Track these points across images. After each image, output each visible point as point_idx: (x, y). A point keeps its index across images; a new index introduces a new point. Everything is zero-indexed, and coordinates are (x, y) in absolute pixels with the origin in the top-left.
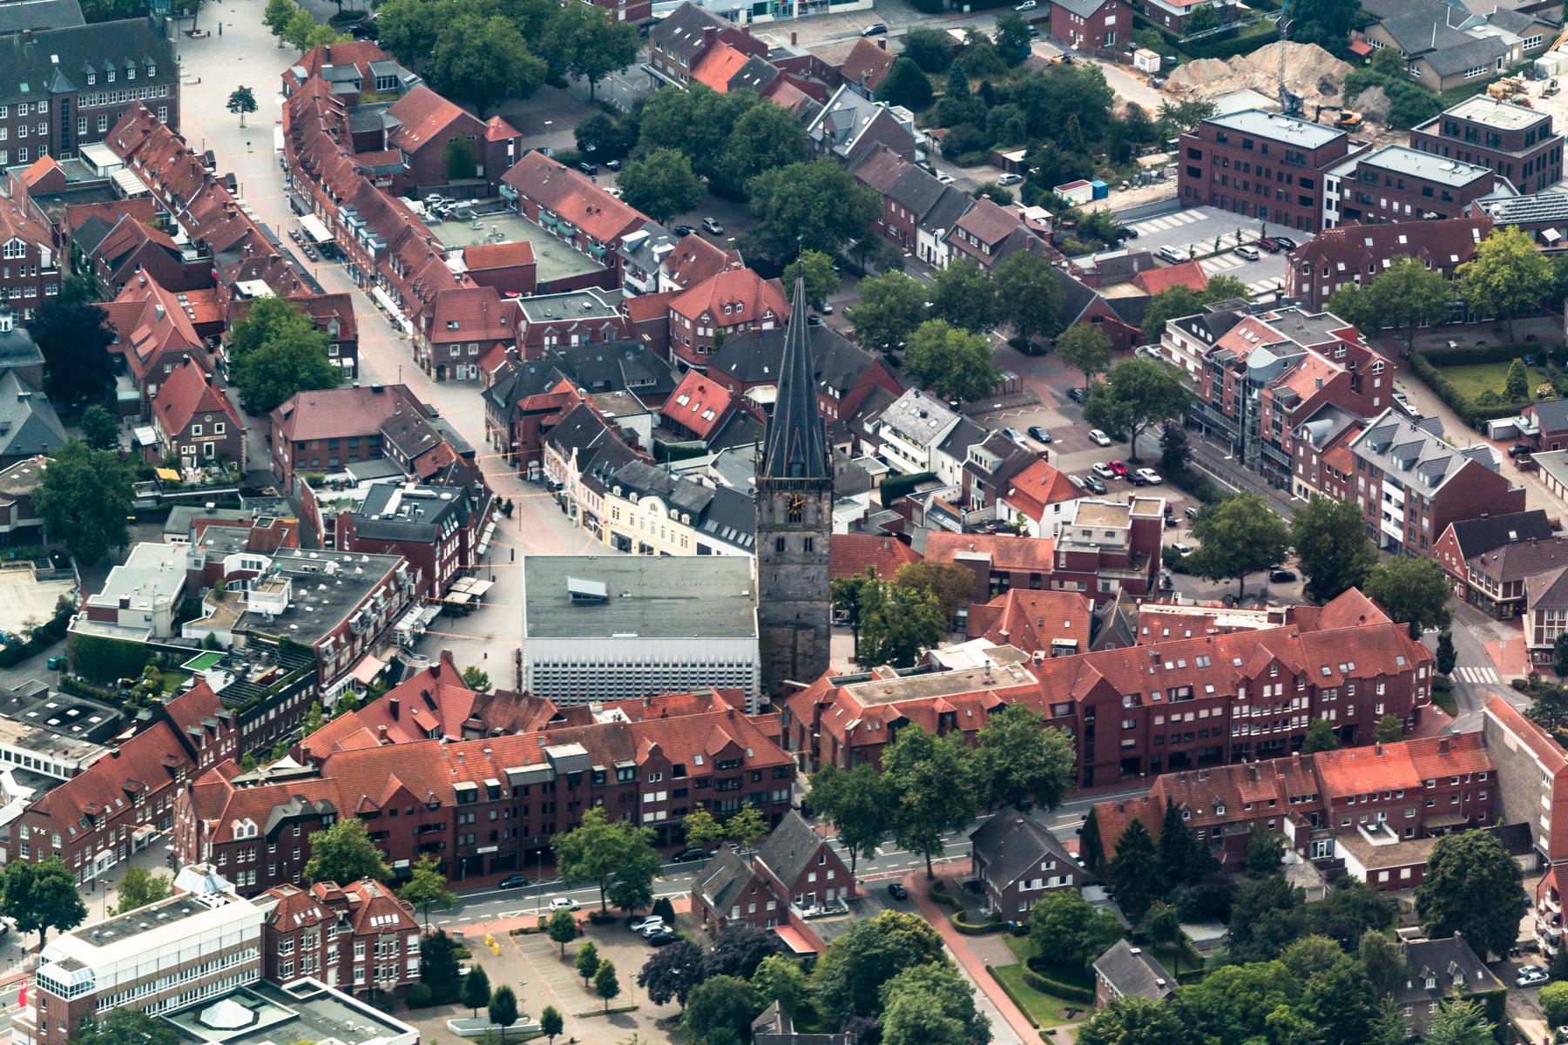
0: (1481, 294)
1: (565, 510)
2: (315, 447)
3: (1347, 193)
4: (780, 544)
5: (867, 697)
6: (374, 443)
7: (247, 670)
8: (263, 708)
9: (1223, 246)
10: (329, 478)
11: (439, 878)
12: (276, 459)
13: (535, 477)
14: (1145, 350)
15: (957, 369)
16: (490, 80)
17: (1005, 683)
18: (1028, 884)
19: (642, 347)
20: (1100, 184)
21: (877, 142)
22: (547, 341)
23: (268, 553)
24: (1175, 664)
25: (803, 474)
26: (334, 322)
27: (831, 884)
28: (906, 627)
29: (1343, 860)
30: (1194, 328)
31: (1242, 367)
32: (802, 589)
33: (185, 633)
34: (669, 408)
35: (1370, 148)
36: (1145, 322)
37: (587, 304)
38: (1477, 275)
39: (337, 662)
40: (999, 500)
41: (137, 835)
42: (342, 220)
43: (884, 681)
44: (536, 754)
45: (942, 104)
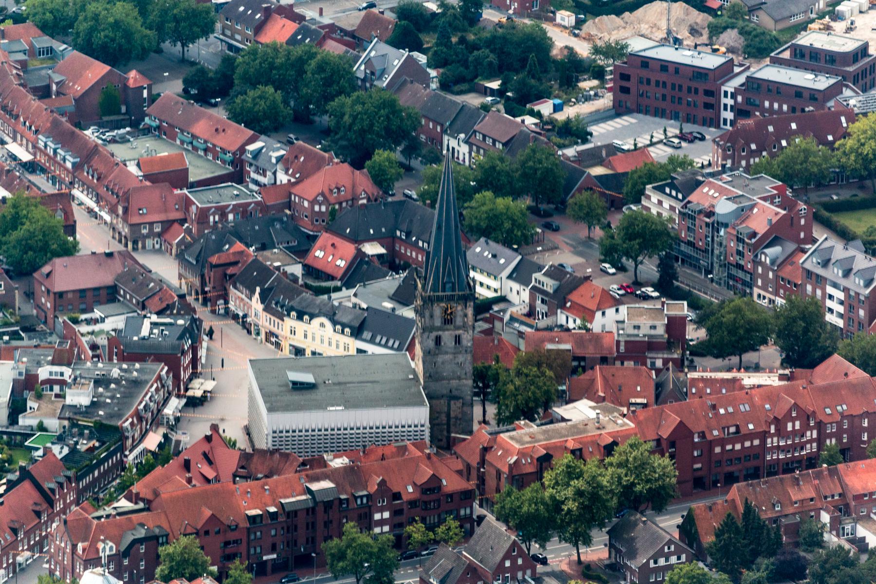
0: (855, 161)
1: (249, 332)
2: (70, 296)
3: (740, 99)
4: (438, 340)
5: (518, 441)
6: (110, 291)
7: (77, 443)
8: (91, 469)
9: (654, 140)
10: (83, 317)
11: (249, 575)
12: (39, 307)
13: (222, 311)
14: (630, 209)
15: (507, 225)
16: (120, 46)
17: (611, 428)
18: (656, 562)
19: (285, 219)
20: (558, 101)
21: (404, 77)
22: (211, 219)
23: (68, 365)
24: (726, 410)
25: (453, 290)
26: (59, 212)
27: (520, 568)
28: (534, 393)
29: (864, 538)
30: (667, 190)
31: (710, 214)
32: (453, 372)
33: (21, 422)
34: (309, 260)
35: (749, 68)
36: (625, 190)
37: (235, 192)
38: (851, 148)
39: (133, 437)
40: (559, 311)
41: (19, 559)
42: (41, 144)
43: (527, 430)
44: (299, 489)
45: (436, 52)
